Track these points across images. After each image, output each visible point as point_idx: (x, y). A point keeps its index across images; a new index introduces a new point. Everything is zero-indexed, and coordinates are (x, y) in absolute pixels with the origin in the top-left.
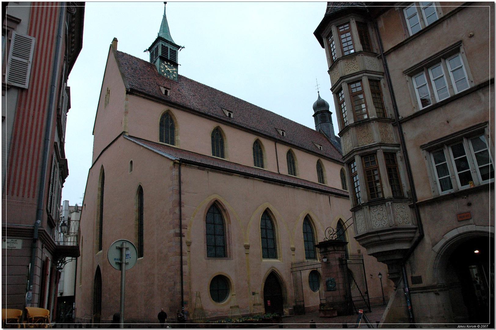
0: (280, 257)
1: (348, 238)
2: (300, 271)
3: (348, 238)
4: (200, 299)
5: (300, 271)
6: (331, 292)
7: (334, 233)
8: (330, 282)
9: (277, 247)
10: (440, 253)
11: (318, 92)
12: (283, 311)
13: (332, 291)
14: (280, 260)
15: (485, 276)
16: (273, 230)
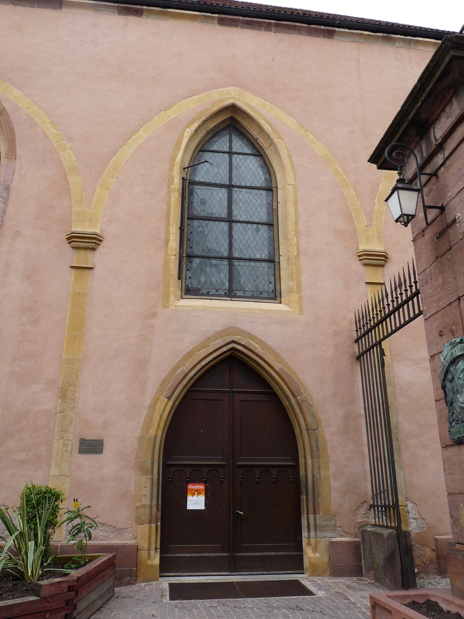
14: (288, 304)
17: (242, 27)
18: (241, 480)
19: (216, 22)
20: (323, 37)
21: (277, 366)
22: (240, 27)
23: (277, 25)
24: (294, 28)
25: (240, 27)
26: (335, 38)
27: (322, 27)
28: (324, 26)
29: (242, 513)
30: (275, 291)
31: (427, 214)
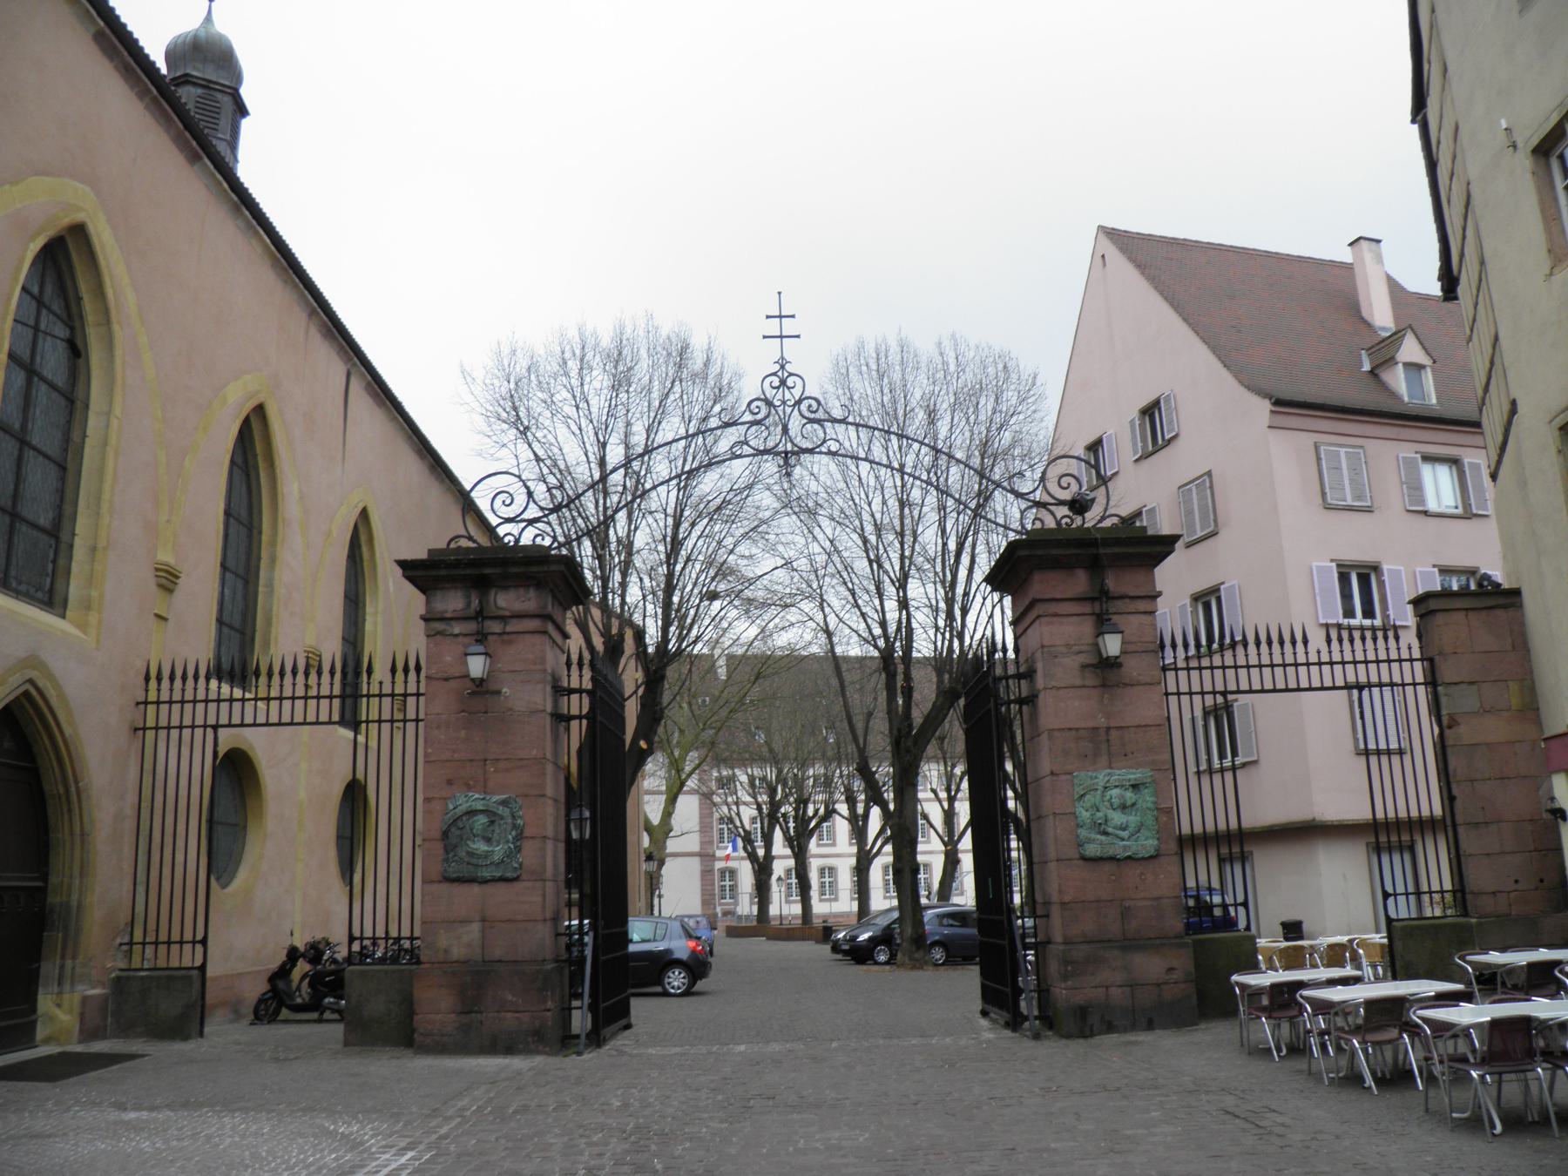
0: (87, 605)
1: (375, 624)
2: (215, 728)
3: (375, 624)
4: (535, 454)
5: (215, 728)
6: (476, 889)
7: (534, 511)
8: (482, 820)
9: (82, 525)
10: (138, 936)
11: (779, 293)
12: (34, 1010)
13: (485, 881)
14: (82, 626)
15: (611, 1001)
16: (73, 400)
17: (116, 67)
18: (1379, 968)
19: (93, 30)
20: (186, 157)
21: (68, 731)
22: (137, 90)
23: (154, 100)
24: (168, 119)
25: (137, 90)
26: (196, 167)
27: (194, 143)
28: (198, 143)
29: (1348, 954)
30: (51, 591)
31: (1195, 996)
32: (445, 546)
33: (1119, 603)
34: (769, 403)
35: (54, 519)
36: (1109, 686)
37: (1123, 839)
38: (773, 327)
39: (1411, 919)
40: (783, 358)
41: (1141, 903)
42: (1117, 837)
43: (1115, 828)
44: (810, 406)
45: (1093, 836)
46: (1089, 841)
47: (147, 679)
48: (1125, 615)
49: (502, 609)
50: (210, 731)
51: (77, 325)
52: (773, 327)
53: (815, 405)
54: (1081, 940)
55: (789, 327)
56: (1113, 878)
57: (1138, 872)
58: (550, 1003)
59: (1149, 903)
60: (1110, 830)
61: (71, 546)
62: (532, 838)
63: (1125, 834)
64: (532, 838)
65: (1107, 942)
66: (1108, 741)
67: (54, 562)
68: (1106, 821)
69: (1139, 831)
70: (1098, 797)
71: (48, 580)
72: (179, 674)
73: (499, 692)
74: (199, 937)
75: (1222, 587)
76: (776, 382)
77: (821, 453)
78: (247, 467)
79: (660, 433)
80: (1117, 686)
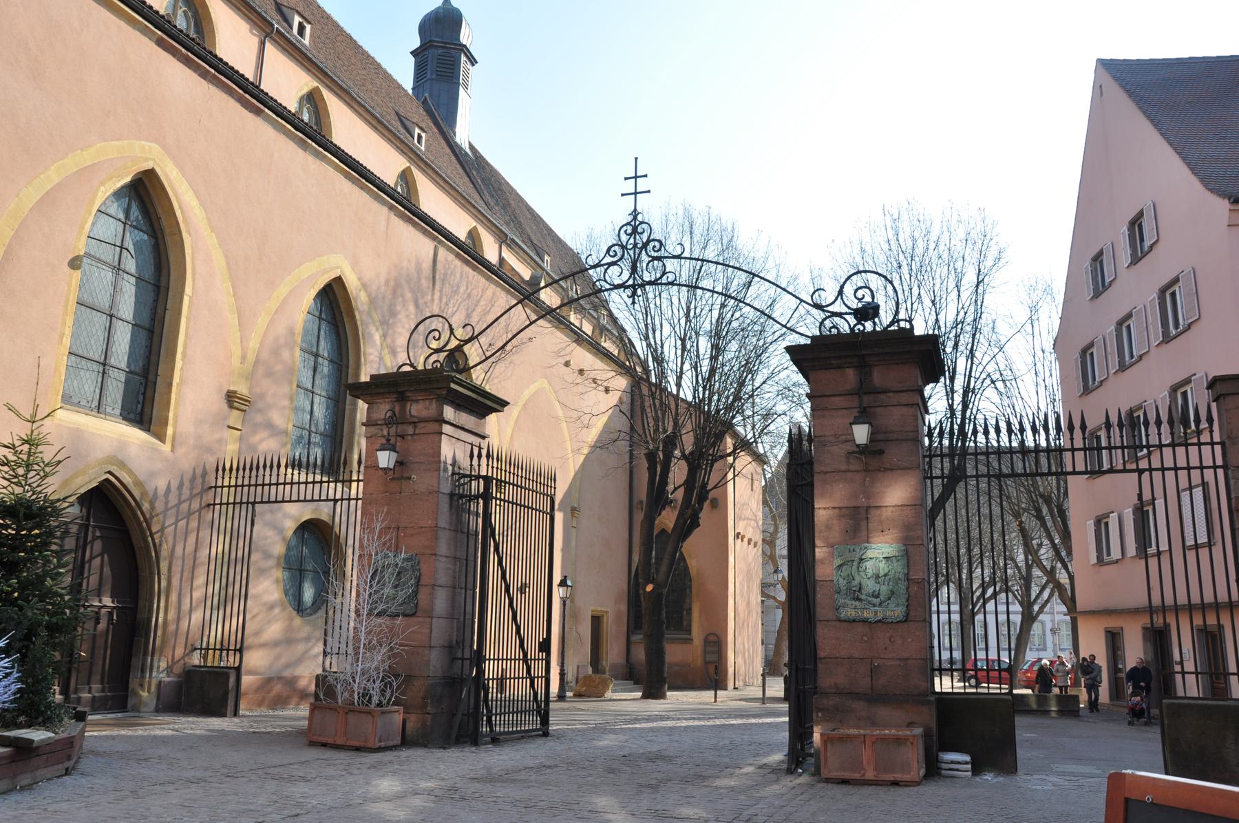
2: (254, 503)
5: (254, 503)
30: (142, 413)
32: (395, 370)
33: (882, 397)
34: (623, 247)
35: (144, 366)
36: (869, 471)
37: (875, 606)
38: (629, 186)
39: (1199, 698)
40: (635, 210)
41: (889, 663)
42: (869, 603)
43: (868, 595)
44: (654, 247)
45: (848, 602)
46: (845, 605)
47: (217, 470)
48: (889, 408)
49: (414, 417)
50: (250, 505)
51: (159, 235)
52: (629, 186)
53: (657, 244)
54: (834, 691)
55: (642, 185)
56: (866, 638)
57: (888, 635)
58: (429, 708)
59: (897, 663)
60: (863, 597)
61: (155, 383)
62: (425, 585)
63: (877, 601)
64: (425, 585)
65: (857, 696)
66: (867, 518)
67: (144, 394)
68: (860, 588)
69: (889, 599)
70: (854, 567)
71: (139, 406)
72: (248, 467)
73: (409, 478)
74: (238, 647)
75: (1193, 378)
76: (629, 230)
77: (662, 284)
78: (336, 322)
79: (451, 257)
80: (879, 470)
